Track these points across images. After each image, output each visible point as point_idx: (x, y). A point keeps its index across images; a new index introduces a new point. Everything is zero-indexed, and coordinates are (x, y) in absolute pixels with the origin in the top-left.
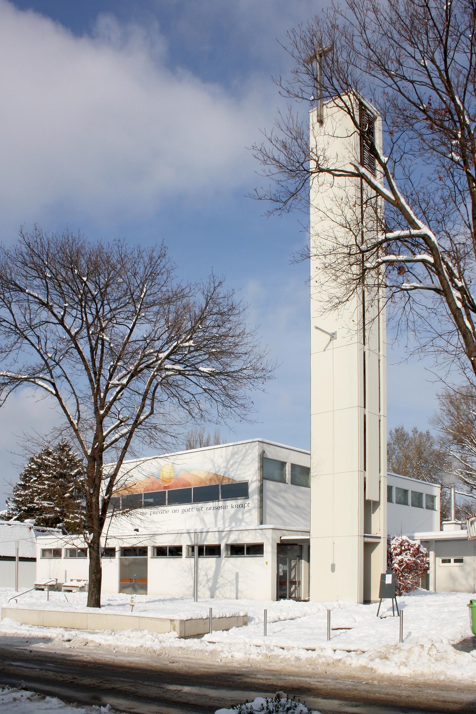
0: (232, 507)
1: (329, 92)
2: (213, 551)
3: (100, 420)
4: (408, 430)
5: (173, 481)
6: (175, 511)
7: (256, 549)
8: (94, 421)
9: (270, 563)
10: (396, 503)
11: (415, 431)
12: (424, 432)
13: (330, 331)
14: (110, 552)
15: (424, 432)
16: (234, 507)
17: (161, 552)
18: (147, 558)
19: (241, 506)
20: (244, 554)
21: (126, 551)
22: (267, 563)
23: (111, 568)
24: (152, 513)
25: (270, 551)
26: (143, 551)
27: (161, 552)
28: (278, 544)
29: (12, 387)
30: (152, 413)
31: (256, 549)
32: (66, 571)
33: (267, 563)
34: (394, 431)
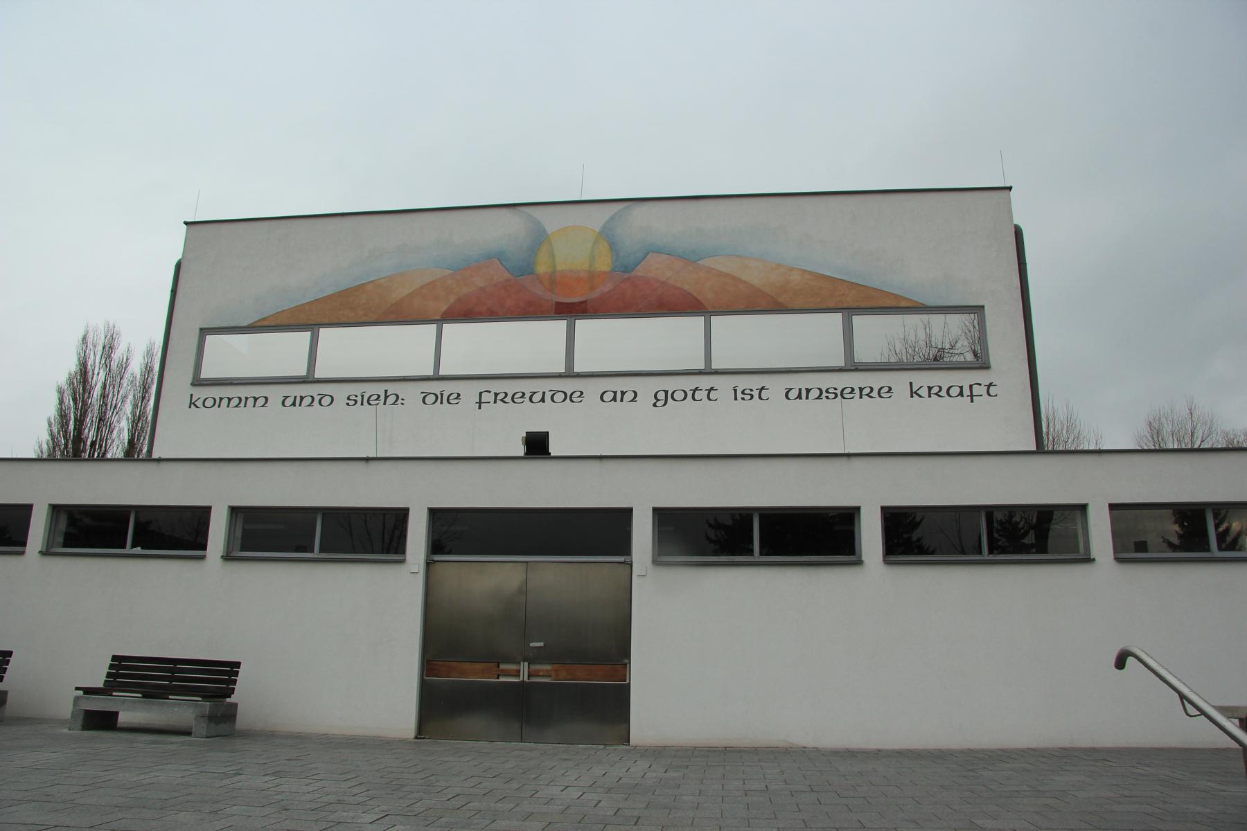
0: (192, 404)
2: (815, 536)
5: (608, 287)
26: (602, 531)
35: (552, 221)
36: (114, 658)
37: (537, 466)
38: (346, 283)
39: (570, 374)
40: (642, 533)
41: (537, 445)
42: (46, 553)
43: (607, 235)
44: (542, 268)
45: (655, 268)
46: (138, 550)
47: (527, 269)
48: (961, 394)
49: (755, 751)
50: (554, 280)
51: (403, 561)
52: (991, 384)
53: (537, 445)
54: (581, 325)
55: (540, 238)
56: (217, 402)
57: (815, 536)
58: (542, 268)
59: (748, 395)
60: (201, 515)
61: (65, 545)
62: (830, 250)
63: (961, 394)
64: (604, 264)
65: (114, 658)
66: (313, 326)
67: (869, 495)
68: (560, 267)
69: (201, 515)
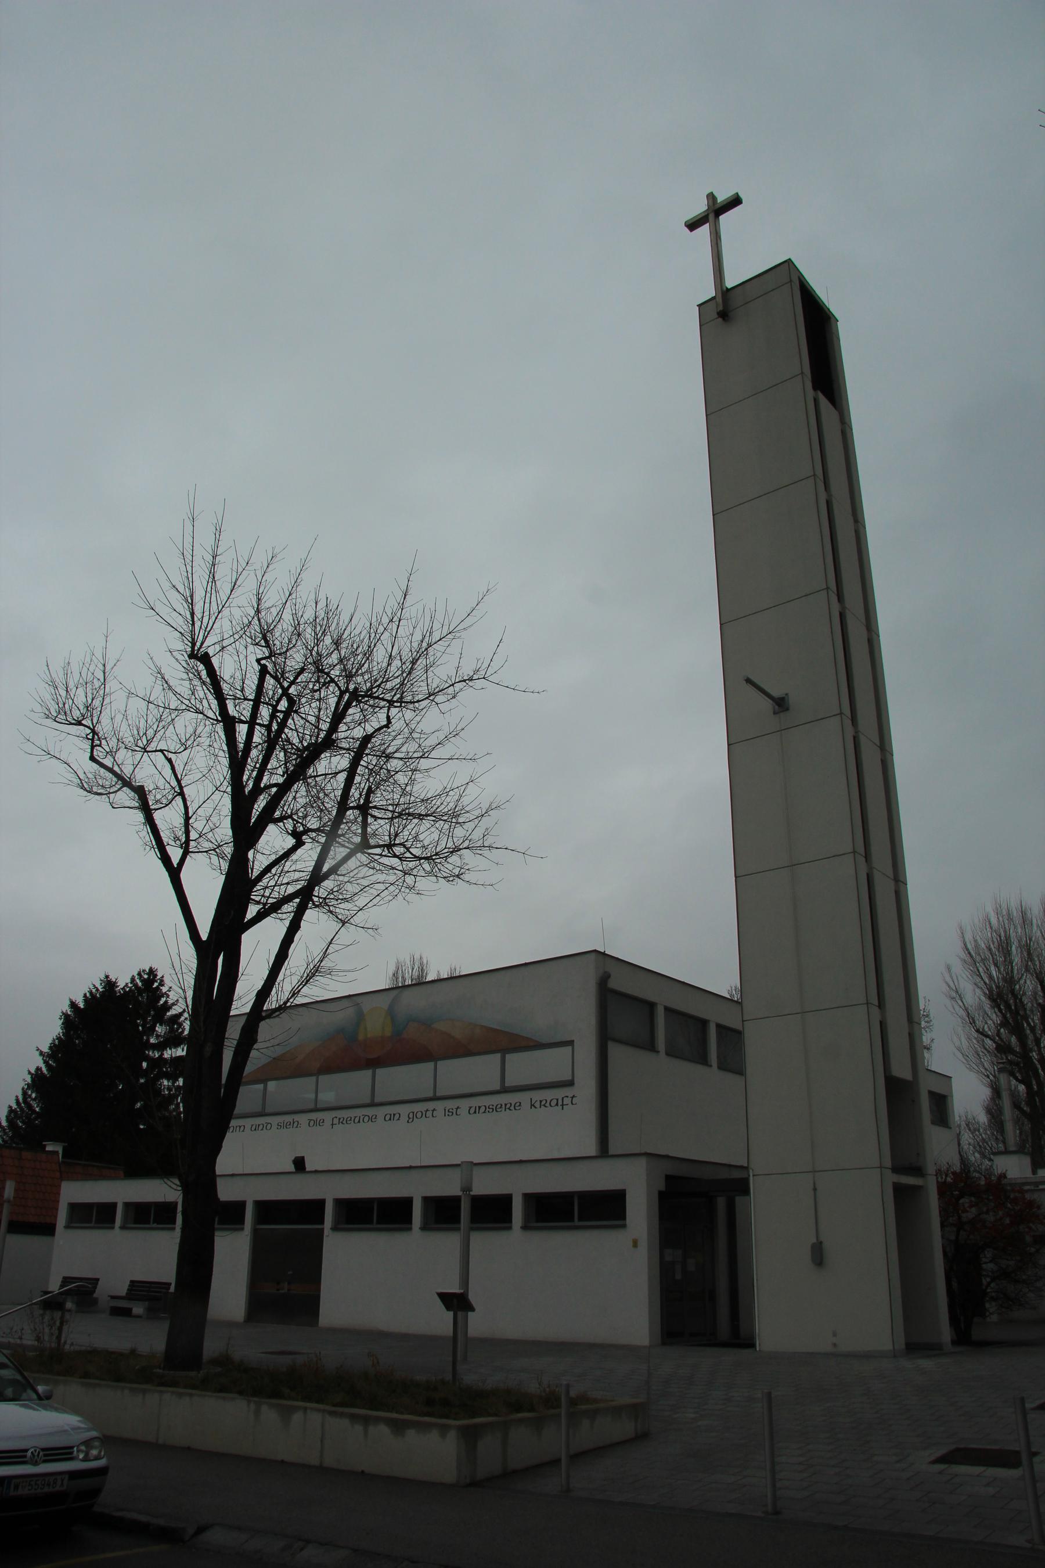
0: (532, 1105)
1: (395, 856)
2: (492, 1211)
3: (246, 833)
7: (604, 1208)
8: (225, 832)
9: (643, 1244)
13: (776, 693)
14: (233, 1214)
16: (537, 1105)
17: (358, 1214)
18: (323, 1229)
19: (554, 1103)
20: (572, 1219)
21: (268, 1210)
22: (635, 1244)
23: (232, 1254)
24: (336, 1121)
26: (312, 1210)
27: (358, 1214)
30: (92, 758)
31: (604, 1208)
32: (748, 681)
33: (635, 1244)
36: (132, 1282)
37: (300, 1177)
39: (505, 1090)
41: (299, 1164)
42: (122, 1228)
43: (391, 1012)
44: (361, 1037)
46: (155, 1225)
48: (557, 1104)
49: (592, 1346)
51: (624, 1226)
52: (434, 1110)
53: (299, 1164)
54: (381, 1072)
55: (360, 1016)
56: (412, 1117)
57: (492, 1211)
58: (361, 1037)
59: (286, 1125)
61: (136, 1222)
63: (557, 1104)
64: (388, 1033)
65: (132, 1282)
68: (369, 1036)
69: (406, 1204)
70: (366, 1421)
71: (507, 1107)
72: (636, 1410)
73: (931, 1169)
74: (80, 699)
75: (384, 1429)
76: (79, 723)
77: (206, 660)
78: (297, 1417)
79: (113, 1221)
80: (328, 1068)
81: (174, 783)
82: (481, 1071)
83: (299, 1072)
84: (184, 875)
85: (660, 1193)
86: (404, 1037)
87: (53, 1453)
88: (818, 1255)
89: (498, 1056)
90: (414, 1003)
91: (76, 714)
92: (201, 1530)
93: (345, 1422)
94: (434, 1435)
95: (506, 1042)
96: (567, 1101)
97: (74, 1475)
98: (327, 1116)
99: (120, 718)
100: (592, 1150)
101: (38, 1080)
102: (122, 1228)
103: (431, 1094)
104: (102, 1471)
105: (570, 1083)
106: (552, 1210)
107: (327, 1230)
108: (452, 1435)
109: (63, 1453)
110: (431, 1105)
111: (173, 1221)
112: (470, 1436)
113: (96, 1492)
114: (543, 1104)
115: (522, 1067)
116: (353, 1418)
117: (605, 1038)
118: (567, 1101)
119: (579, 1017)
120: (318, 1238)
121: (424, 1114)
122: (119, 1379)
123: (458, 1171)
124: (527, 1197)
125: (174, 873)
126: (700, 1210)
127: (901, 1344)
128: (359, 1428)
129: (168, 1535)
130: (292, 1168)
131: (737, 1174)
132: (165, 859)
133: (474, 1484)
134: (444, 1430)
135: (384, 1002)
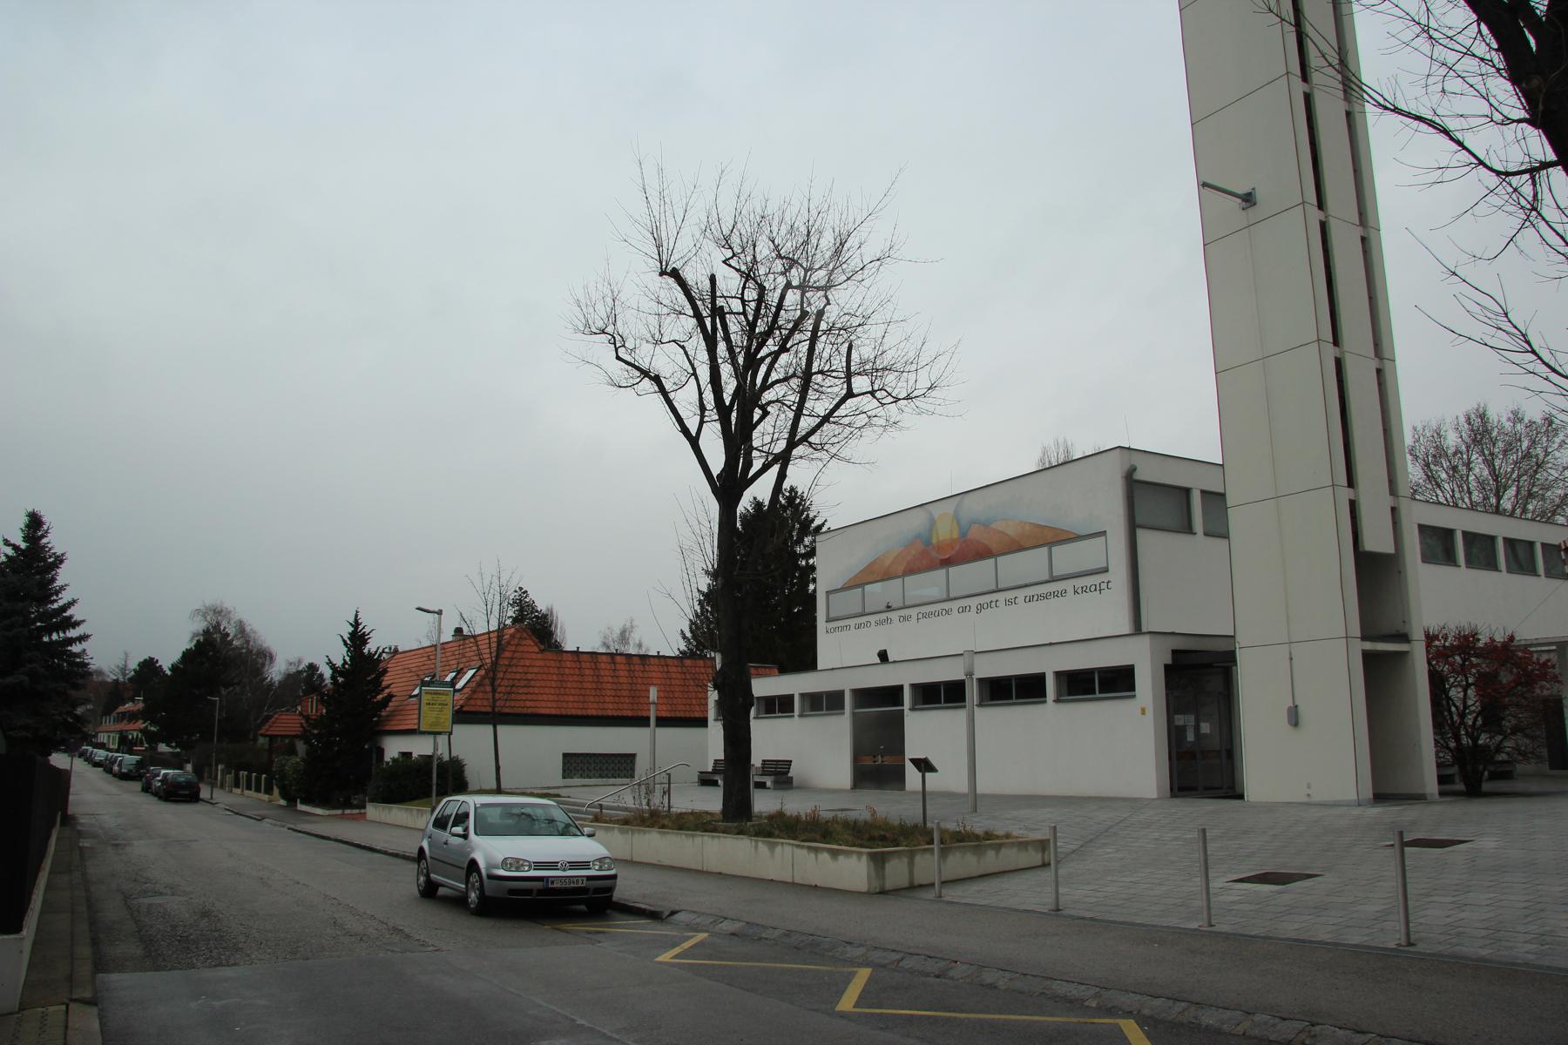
2: (1027, 688)
4: (1498, 414)
5: (957, 547)
6: (964, 609)
7: (1118, 681)
10: (1206, 534)
11: (1516, 417)
12: (1538, 418)
13: (1241, 191)
15: (1538, 418)
21: (866, 697)
22: (1143, 711)
25: (1148, 683)
26: (892, 695)
28: (1166, 666)
29: (686, 399)
30: (618, 358)
31: (1118, 681)
33: (1143, 711)
34: (1462, 420)
35: (936, 511)
37: (885, 667)
38: (871, 560)
39: (1053, 580)
40: (653, 721)
41: (883, 656)
44: (934, 541)
45: (975, 533)
47: (928, 543)
50: (939, 548)
53: (883, 656)
55: (932, 523)
56: (980, 608)
57: (1027, 688)
59: (859, 627)
60: (1040, 678)
62: (1039, 510)
64: (955, 536)
66: (862, 585)
67: (1049, 665)
69: (1040, 678)
70: (816, 850)
71: (1055, 594)
72: (1043, 845)
73: (1418, 635)
74: (602, 311)
75: (825, 856)
76: (603, 332)
77: (675, 274)
78: (778, 849)
79: (1044, 694)
80: (910, 571)
81: (687, 365)
82: (1030, 563)
83: (887, 576)
84: (701, 442)
85: (1166, 666)
86: (953, 545)
87: (574, 865)
88: (1294, 717)
89: (1045, 549)
90: (973, 508)
91: (600, 324)
92: (673, 913)
93: (805, 851)
94: (854, 858)
95: (1052, 538)
96: (1104, 586)
97: (589, 878)
98: (913, 612)
99: (633, 326)
100: (1125, 627)
101: (709, 597)
102: (801, 716)
103: (993, 587)
104: (614, 877)
105: (1106, 570)
106: (1079, 684)
107: (906, 712)
108: (864, 858)
109: (584, 865)
110: (994, 597)
111: (843, 707)
112: (879, 861)
113: (610, 889)
114: (1084, 590)
115: (1067, 557)
116: (809, 848)
117: (1133, 526)
118: (1104, 586)
119: (1110, 510)
120: (899, 720)
121: (989, 605)
122: (681, 828)
123: (960, 660)
124: (1058, 674)
125: (694, 442)
126: (1200, 678)
127: (1368, 793)
128: (813, 855)
129: (654, 915)
130: (878, 660)
131: (1222, 646)
132: (685, 431)
133: (883, 892)
134: (860, 854)
135: (950, 507)
